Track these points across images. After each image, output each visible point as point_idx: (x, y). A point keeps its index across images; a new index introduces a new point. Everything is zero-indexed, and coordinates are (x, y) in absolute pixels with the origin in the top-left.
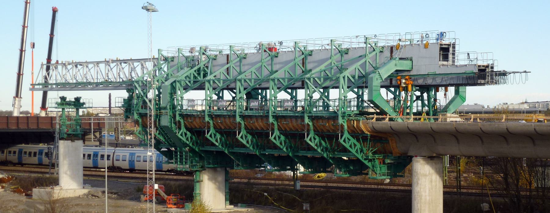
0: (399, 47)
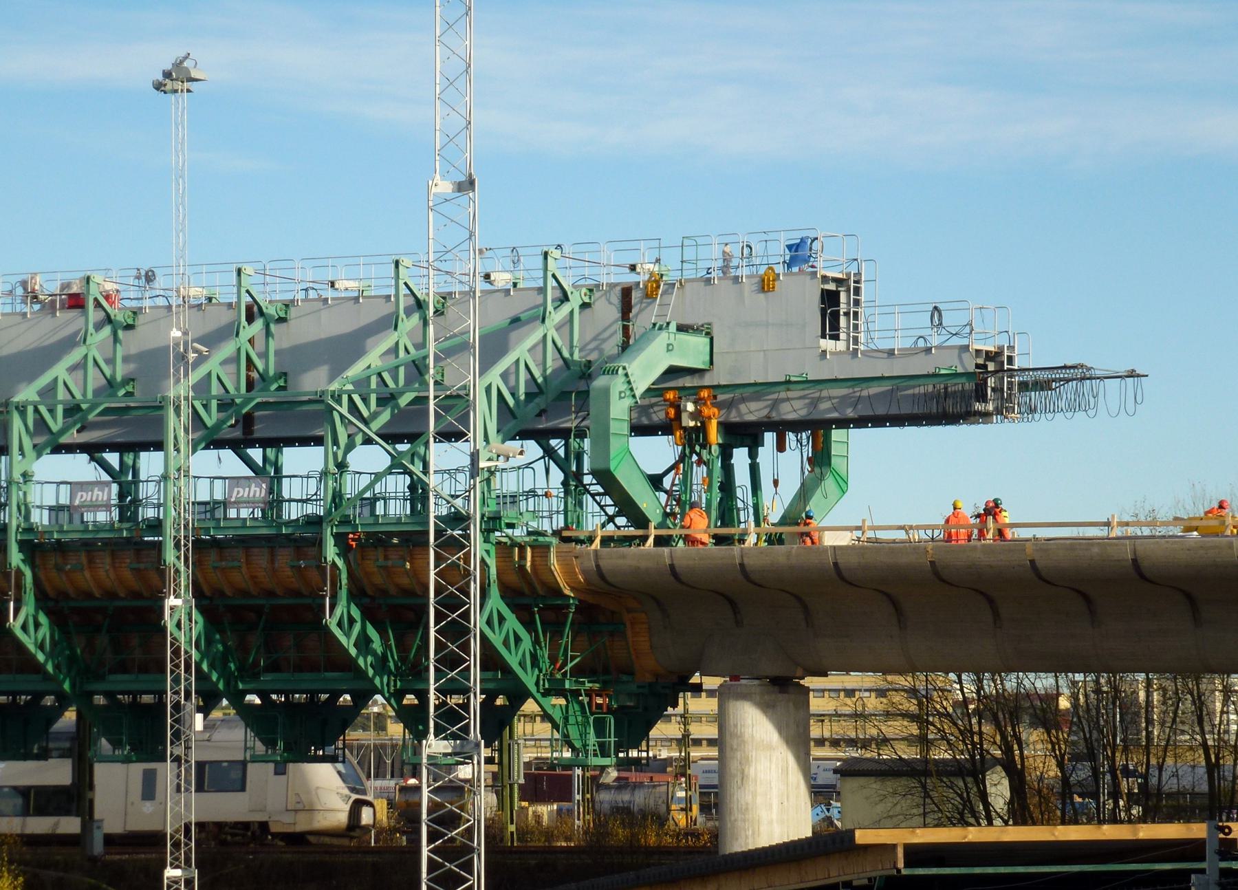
0: (658, 287)
